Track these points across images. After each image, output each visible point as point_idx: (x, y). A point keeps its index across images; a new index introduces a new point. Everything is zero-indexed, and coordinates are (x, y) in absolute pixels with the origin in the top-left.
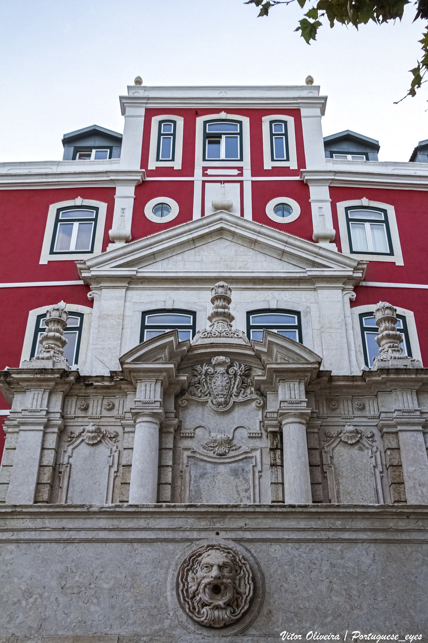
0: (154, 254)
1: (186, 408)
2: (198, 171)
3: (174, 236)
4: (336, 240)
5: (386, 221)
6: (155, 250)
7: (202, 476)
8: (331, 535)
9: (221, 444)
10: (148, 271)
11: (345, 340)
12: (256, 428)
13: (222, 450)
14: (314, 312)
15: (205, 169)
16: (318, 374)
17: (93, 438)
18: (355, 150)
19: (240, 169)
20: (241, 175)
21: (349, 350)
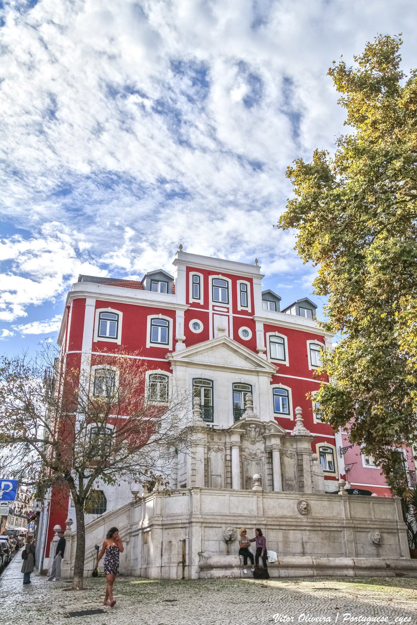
2: (210, 307)
4: (265, 353)
5: (284, 344)
7: (248, 464)
12: (263, 449)
13: (253, 456)
15: (213, 306)
18: (271, 300)
19: (228, 308)
20: (228, 312)
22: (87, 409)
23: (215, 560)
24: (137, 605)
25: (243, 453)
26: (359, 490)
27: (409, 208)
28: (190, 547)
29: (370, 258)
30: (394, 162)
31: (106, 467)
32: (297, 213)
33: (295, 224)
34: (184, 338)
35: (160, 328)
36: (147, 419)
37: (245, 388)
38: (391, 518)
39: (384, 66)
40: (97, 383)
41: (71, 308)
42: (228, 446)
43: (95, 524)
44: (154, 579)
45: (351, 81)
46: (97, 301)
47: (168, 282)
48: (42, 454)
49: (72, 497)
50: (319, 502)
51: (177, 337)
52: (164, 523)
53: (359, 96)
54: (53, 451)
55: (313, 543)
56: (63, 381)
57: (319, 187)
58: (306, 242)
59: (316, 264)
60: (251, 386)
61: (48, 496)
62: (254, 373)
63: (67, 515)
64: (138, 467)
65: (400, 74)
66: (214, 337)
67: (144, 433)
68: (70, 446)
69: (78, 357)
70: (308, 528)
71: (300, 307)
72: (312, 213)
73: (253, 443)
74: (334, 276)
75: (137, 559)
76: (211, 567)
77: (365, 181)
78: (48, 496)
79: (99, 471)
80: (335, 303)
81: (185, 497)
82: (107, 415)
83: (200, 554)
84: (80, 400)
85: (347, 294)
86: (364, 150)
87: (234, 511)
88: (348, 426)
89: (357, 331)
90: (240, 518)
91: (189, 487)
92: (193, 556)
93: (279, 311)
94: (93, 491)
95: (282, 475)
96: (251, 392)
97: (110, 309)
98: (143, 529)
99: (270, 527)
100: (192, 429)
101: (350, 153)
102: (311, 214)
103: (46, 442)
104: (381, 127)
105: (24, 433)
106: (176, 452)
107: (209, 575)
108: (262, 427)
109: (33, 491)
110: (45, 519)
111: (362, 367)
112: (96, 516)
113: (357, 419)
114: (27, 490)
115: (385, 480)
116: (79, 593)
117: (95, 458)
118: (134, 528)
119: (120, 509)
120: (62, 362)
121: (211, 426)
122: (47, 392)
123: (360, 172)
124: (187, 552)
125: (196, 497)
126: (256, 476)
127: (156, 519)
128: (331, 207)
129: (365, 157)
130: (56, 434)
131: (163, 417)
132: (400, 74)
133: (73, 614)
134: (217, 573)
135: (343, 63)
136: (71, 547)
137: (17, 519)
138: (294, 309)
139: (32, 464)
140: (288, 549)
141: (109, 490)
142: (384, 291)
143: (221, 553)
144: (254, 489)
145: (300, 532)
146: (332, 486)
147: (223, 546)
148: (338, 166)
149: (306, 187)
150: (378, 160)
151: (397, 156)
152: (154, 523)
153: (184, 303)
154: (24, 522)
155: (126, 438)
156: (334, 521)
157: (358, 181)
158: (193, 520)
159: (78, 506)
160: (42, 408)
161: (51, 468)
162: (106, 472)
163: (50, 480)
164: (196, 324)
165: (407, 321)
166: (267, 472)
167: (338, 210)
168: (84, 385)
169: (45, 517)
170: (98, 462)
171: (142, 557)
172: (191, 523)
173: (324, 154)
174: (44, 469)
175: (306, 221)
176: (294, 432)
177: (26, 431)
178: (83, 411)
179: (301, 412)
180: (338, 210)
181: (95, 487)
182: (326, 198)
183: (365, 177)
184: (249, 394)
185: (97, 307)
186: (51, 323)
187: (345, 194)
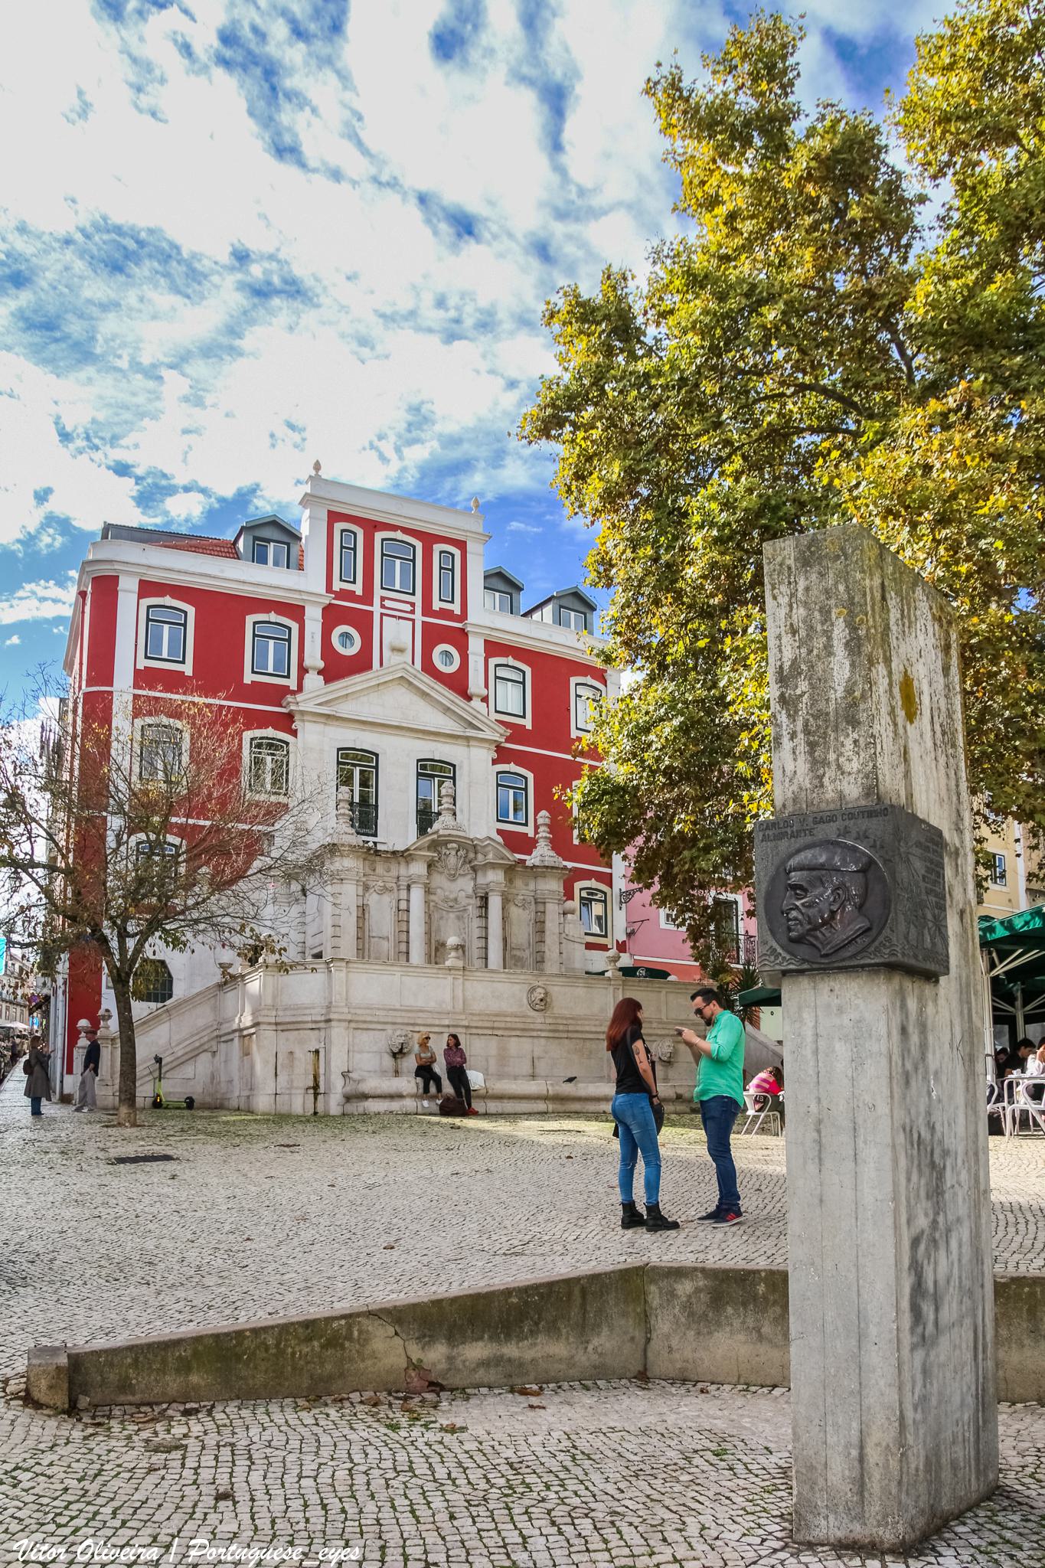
2: (377, 601)
4: (485, 699)
5: (523, 683)
7: (441, 918)
12: (470, 891)
15: (383, 599)
16: (275, 523)
19: (413, 605)
20: (413, 612)
22: (126, 808)
23: (371, 1085)
24: (230, 1150)
25: (432, 897)
26: (648, 970)
27: (791, 411)
28: (327, 1063)
29: (697, 518)
30: (764, 310)
31: (167, 918)
32: (559, 408)
33: (553, 432)
34: (321, 664)
35: (271, 642)
36: (247, 827)
37: (441, 769)
39: (764, 86)
40: (147, 751)
41: (89, 596)
42: (403, 883)
43: (151, 1020)
44: (263, 1114)
45: (692, 113)
46: (141, 582)
47: (288, 545)
48: (47, 892)
49: (106, 971)
50: (567, 989)
51: (307, 663)
52: (279, 1020)
53: (704, 150)
54: (66, 886)
56: (78, 751)
57: (609, 352)
58: (575, 474)
59: (593, 523)
60: (454, 766)
61: (63, 967)
62: (460, 742)
63: (99, 1003)
64: (227, 919)
65: (795, 109)
66: (381, 664)
67: (238, 855)
68: (98, 877)
69: (106, 699)
70: (543, 1034)
71: (561, 607)
72: (591, 409)
73: (453, 878)
74: (624, 552)
75: (231, 1081)
76: (365, 1097)
77: (703, 347)
78: (63, 967)
79: (153, 926)
80: (623, 608)
81: (314, 975)
82: (166, 817)
83: (345, 1075)
84: (112, 788)
85: (646, 590)
86: (706, 276)
87: (410, 1001)
88: (631, 851)
89: (662, 666)
90: (420, 1015)
91: (326, 957)
92: (333, 1077)
93: (518, 613)
94: (145, 960)
95: (505, 940)
96: (454, 778)
97: (168, 600)
98: (241, 1030)
99: (474, 1031)
100: (332, 849)
101: (677, 283)
102: (590, 411)
103: (51, 867)
104: (747, 227)
105: (10, 852)
106: (304, 892)
107: (361, 1110)
108: (471, 849)
109: (34, 957)
110: (60, 1008)
111: (663, 740)
112: (153, 1005)
113: (648, 839)
114: (24, 956)
115: (691, 951)
116: (130, 1132)
117: (146, 901)
118: (225, 1028)
119: (198, 994)
120: (75, 711)
121: (371, 844)
122: (48, 772)
123: (694, 327)
124: (322, 1071)
125: (339, 974)
126: (452, 941)
127: (265, 1012)
128: (630, 399)
129: (706, 294)
130: (71, 855)
131: (277, 826)
132: (795, 109)
133: (121, 1160)
134: (373, 1106)
135: (677, 67)
136: (110, 1058)
137: (7, 1009)
138: (548, 610)
139: (29, 908)
140: (506, 1069)
141: (176, 961)
142: (717, 588)
143: (383, 1073)
144: (448, 963)
145: (530, 1040)
146: (598, 961)
147: (389, 1061)
148: (653, 306)
149: (581, 353)
150: (733, 304)
151: (771, 299)
152: (260, 1019)
153: (322, 590)
154: (22, 1013)
155: (207, 863)
157: (689, 347)
158: (332, 1016)
159: (120, 986)
160: (39, 803)
161: (65, 916)
162: (168, 927)
163: (64, 939)
164: (346, 636)
165: (747, 658)
166: (477, 933)
167: (644, 409)
168: (120, 759)
169: (60, 1005)
170: (150, 909)
171: (241, 1078)
172: (328, 1021)
173: (625, 279)
174: (53, 919)
175: (576, 426)
176: (531, 860)
177: (12, 846)
178: (120, 811)
179: (547, 821)
180: (644, 409)
181: (148, 952)
182: (622, 378)
183: (703, 339)
184: (448, 783)
185: (142, 594)
186: (15, 602)
187: (659, 374)
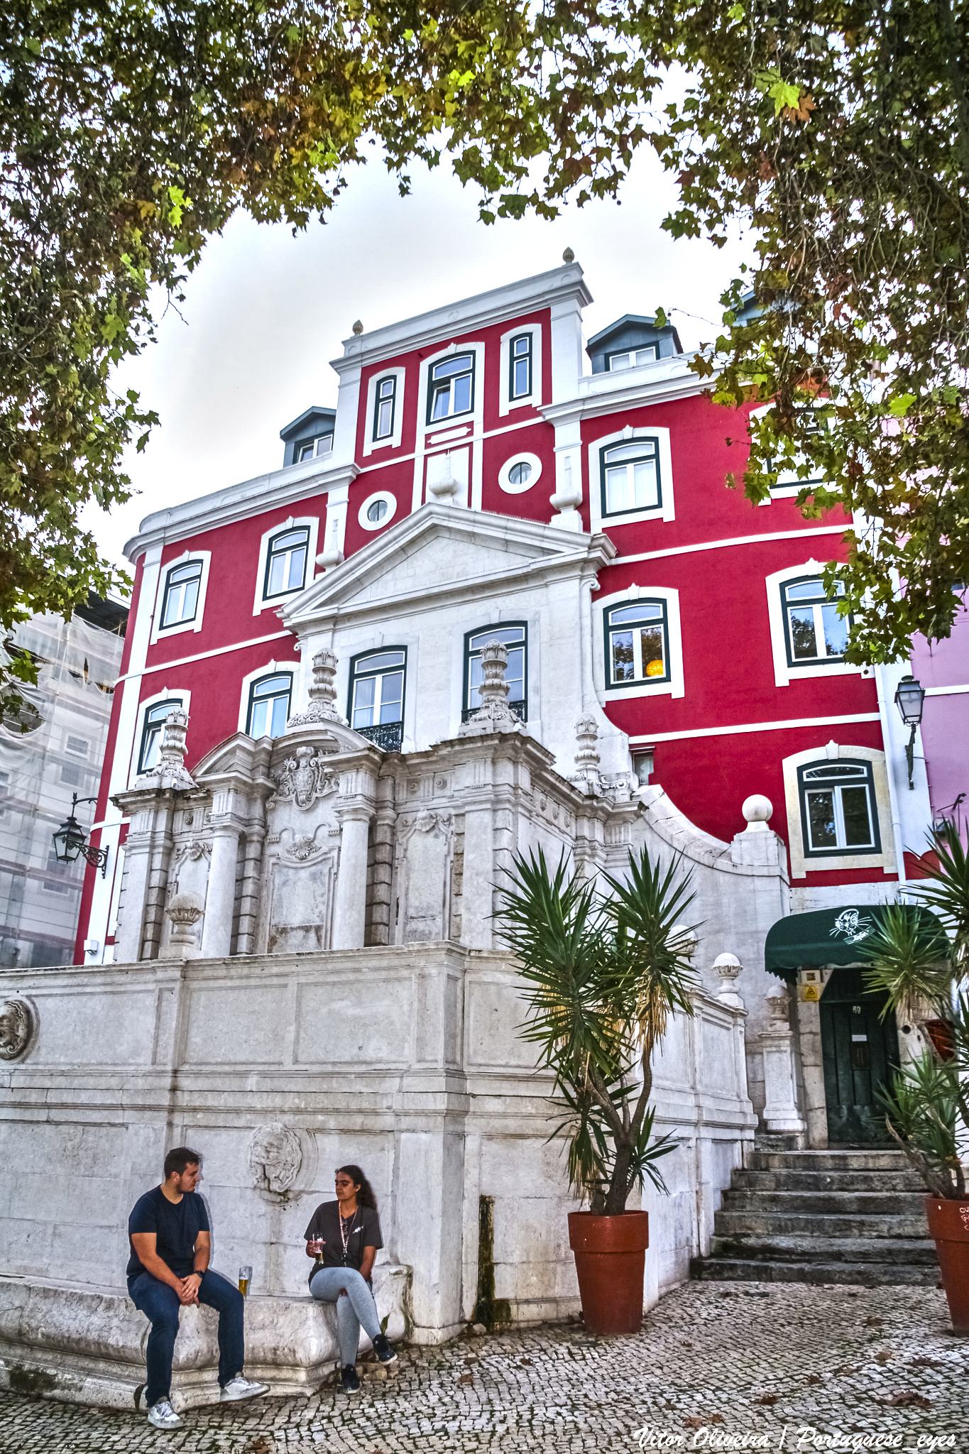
0: (358, 580)
1: (273, 810)
3: (378, 551)
6: (357, 574)
7: (285, 883)
8: (79, 990)
9: (300, 847)
10: (349, 606)
11: (578, 651)
14: (544, 620)
17: (193, 854)
18: (641, 342)
19: (470, 424)
21: (582, 664)
38: (383, 1054)
55: (16, 1175)
156: (103, 1083)
